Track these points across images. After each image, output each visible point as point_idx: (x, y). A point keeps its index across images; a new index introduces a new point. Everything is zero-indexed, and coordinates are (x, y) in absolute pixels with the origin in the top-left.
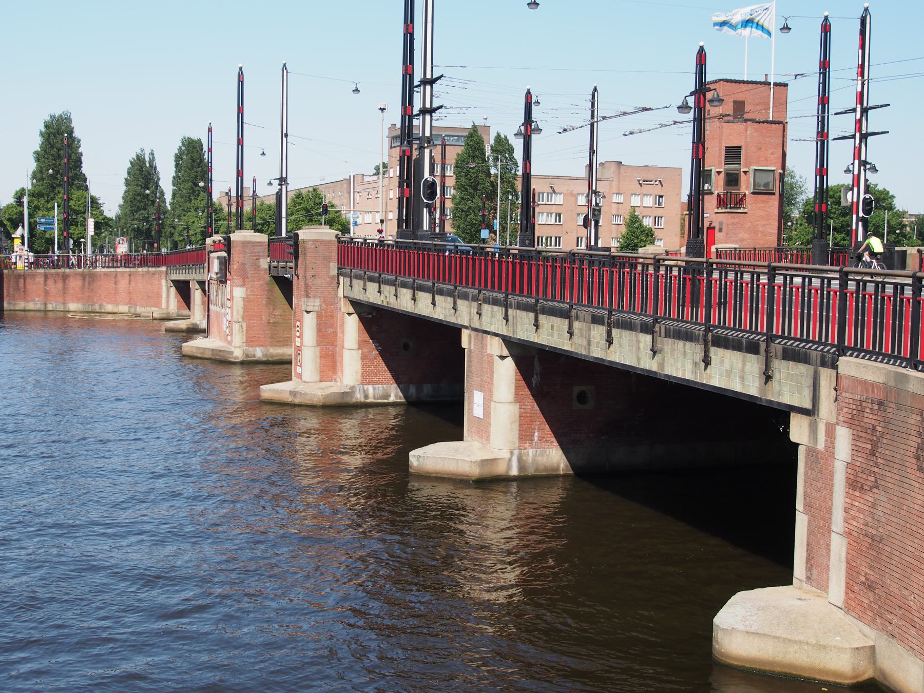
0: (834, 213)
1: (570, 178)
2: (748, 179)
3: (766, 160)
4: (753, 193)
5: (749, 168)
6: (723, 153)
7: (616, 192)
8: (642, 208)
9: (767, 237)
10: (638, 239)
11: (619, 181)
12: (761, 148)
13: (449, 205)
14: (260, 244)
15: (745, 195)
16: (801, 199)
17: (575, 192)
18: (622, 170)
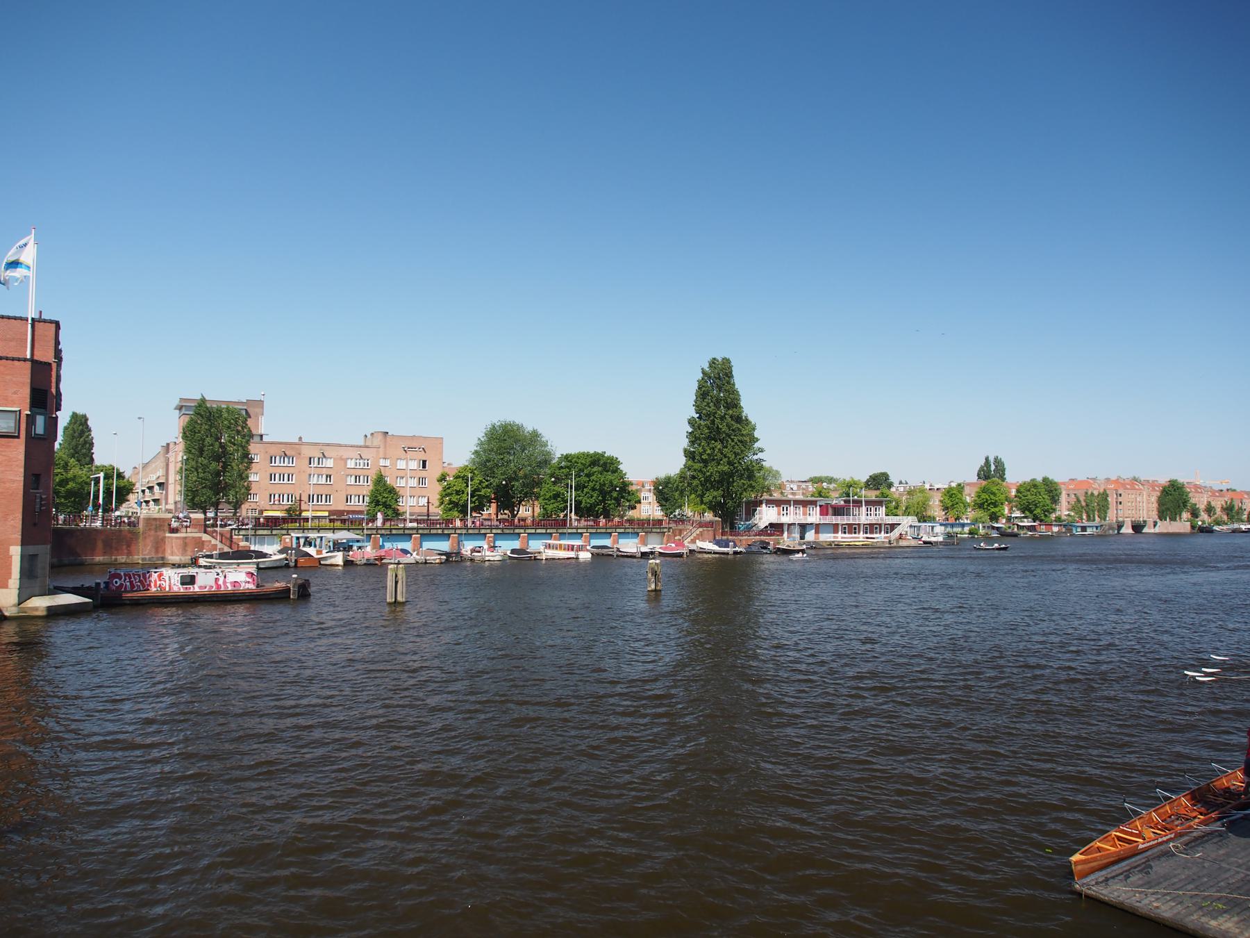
1: (340, 446)
9: (7, 485)
11: (385, 447)
17: (344, 457)
18: (388, 439)
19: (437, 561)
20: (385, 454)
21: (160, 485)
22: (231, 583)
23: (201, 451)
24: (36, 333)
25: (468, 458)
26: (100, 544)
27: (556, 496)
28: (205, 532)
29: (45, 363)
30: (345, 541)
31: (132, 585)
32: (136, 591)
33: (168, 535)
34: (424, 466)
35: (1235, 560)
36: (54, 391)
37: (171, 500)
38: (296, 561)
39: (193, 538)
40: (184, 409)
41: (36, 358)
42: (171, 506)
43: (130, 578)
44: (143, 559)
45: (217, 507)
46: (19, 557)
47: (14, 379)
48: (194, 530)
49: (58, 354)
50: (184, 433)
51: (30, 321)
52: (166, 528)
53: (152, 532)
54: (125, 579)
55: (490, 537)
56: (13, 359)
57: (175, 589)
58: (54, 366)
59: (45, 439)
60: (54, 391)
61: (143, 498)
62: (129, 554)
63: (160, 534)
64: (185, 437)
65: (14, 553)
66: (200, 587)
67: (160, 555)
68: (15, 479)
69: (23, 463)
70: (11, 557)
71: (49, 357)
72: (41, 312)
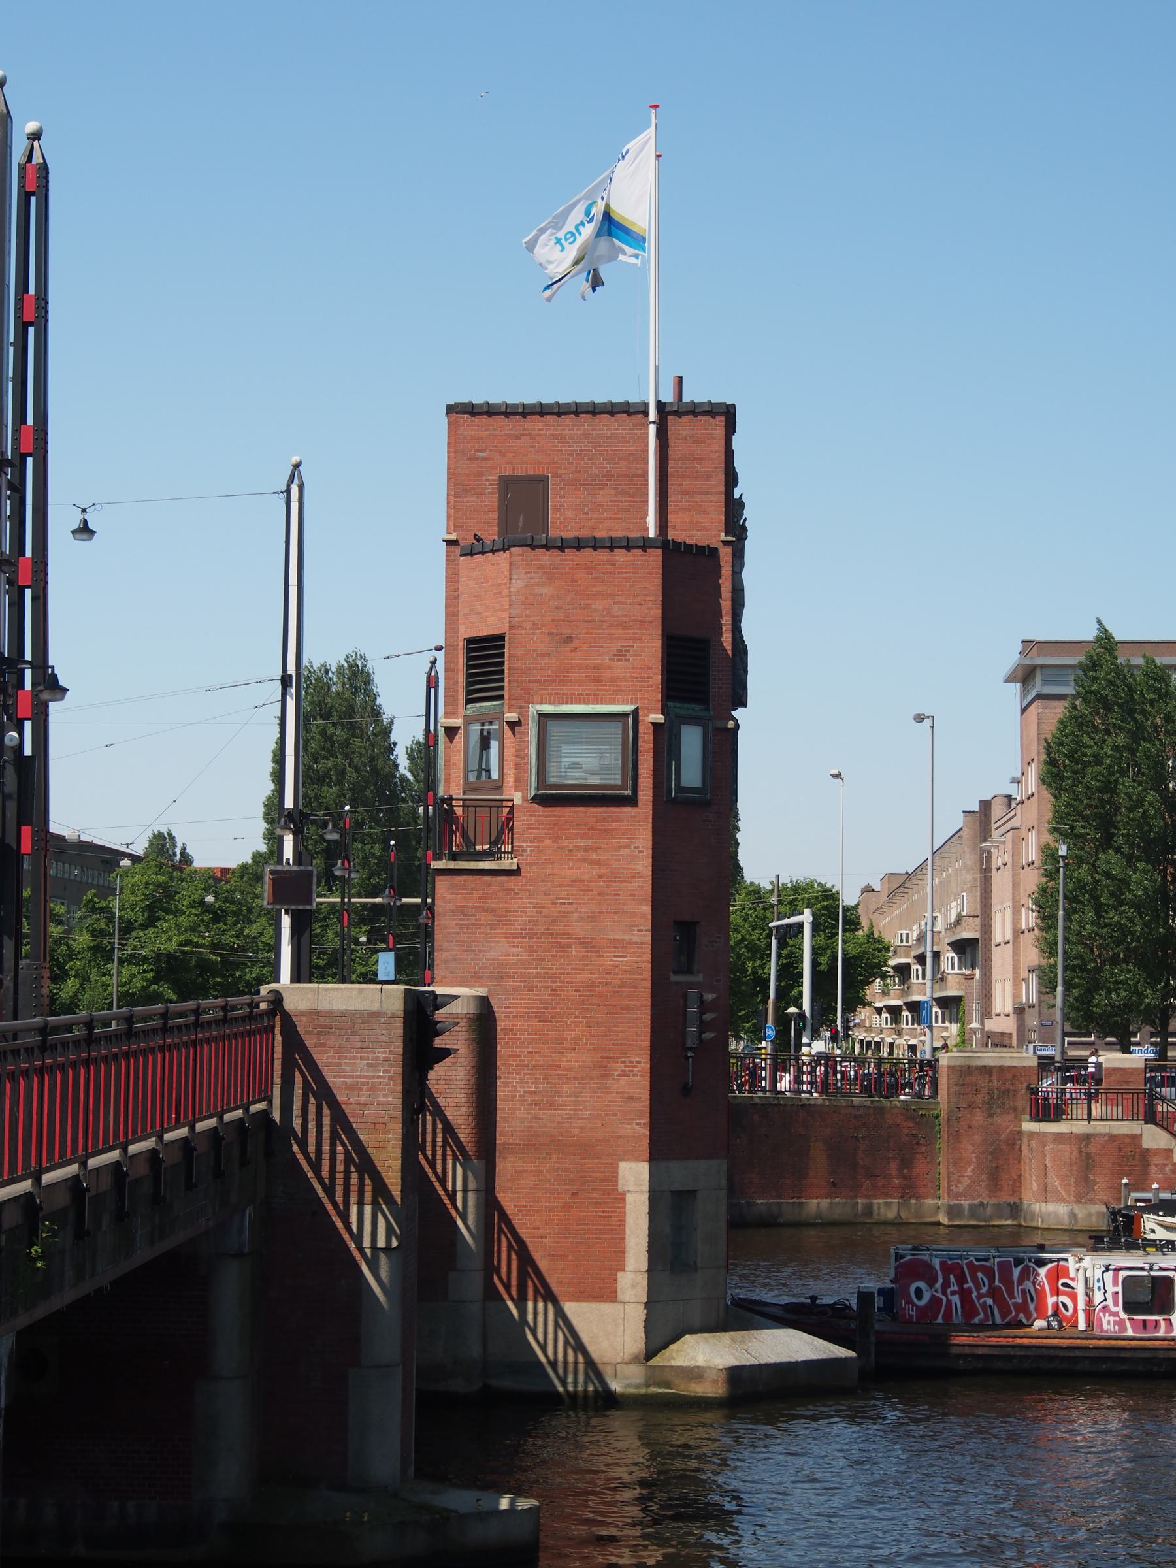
2: (521, 753)
3: (596, 679)
5: (523, 709)
9: (607, 960)
14: (647, 530)
21: (963, 947)
23: (1106, 825)
24: (671, 452)
26: (819, 1157)
28: (1151, 1117)
29: (701, 549)
31: (969, 1308)
32: (982, 1327)
33: (1028, 1126)
35: (1175, 1061)
36: (727, 640)
37: (1003, 1000)
39: (1113, 1138)
40: (1038, 679)
41: (672, 535)
42: (1004, 1024)
43: (961, 1280)
44: (953, 1211)
45: (1165, 1024)
46: (644, 1198)
47: (616, 610)
48: (1114, 1111)
49: (734, 510)
50: (1052, 762)
51: (652, 416)
52: (1023, 1102)
53: (979, 1118)
54: (946, 1284)
56: (612, 545)
57: (1108, 1324)
58: (725, 555)
59: (706, 804)
60: (727, 640)
61: (904, 993)
62: (909, 1190)
63: (1003, 1121)
64: (1053, 776)
65: (631, 1186)
67: (1006, 1198)
68: (627, 938)
69: (646, 886)
70: (622, 1198)
71: (713, 534)
72: (680, 381)
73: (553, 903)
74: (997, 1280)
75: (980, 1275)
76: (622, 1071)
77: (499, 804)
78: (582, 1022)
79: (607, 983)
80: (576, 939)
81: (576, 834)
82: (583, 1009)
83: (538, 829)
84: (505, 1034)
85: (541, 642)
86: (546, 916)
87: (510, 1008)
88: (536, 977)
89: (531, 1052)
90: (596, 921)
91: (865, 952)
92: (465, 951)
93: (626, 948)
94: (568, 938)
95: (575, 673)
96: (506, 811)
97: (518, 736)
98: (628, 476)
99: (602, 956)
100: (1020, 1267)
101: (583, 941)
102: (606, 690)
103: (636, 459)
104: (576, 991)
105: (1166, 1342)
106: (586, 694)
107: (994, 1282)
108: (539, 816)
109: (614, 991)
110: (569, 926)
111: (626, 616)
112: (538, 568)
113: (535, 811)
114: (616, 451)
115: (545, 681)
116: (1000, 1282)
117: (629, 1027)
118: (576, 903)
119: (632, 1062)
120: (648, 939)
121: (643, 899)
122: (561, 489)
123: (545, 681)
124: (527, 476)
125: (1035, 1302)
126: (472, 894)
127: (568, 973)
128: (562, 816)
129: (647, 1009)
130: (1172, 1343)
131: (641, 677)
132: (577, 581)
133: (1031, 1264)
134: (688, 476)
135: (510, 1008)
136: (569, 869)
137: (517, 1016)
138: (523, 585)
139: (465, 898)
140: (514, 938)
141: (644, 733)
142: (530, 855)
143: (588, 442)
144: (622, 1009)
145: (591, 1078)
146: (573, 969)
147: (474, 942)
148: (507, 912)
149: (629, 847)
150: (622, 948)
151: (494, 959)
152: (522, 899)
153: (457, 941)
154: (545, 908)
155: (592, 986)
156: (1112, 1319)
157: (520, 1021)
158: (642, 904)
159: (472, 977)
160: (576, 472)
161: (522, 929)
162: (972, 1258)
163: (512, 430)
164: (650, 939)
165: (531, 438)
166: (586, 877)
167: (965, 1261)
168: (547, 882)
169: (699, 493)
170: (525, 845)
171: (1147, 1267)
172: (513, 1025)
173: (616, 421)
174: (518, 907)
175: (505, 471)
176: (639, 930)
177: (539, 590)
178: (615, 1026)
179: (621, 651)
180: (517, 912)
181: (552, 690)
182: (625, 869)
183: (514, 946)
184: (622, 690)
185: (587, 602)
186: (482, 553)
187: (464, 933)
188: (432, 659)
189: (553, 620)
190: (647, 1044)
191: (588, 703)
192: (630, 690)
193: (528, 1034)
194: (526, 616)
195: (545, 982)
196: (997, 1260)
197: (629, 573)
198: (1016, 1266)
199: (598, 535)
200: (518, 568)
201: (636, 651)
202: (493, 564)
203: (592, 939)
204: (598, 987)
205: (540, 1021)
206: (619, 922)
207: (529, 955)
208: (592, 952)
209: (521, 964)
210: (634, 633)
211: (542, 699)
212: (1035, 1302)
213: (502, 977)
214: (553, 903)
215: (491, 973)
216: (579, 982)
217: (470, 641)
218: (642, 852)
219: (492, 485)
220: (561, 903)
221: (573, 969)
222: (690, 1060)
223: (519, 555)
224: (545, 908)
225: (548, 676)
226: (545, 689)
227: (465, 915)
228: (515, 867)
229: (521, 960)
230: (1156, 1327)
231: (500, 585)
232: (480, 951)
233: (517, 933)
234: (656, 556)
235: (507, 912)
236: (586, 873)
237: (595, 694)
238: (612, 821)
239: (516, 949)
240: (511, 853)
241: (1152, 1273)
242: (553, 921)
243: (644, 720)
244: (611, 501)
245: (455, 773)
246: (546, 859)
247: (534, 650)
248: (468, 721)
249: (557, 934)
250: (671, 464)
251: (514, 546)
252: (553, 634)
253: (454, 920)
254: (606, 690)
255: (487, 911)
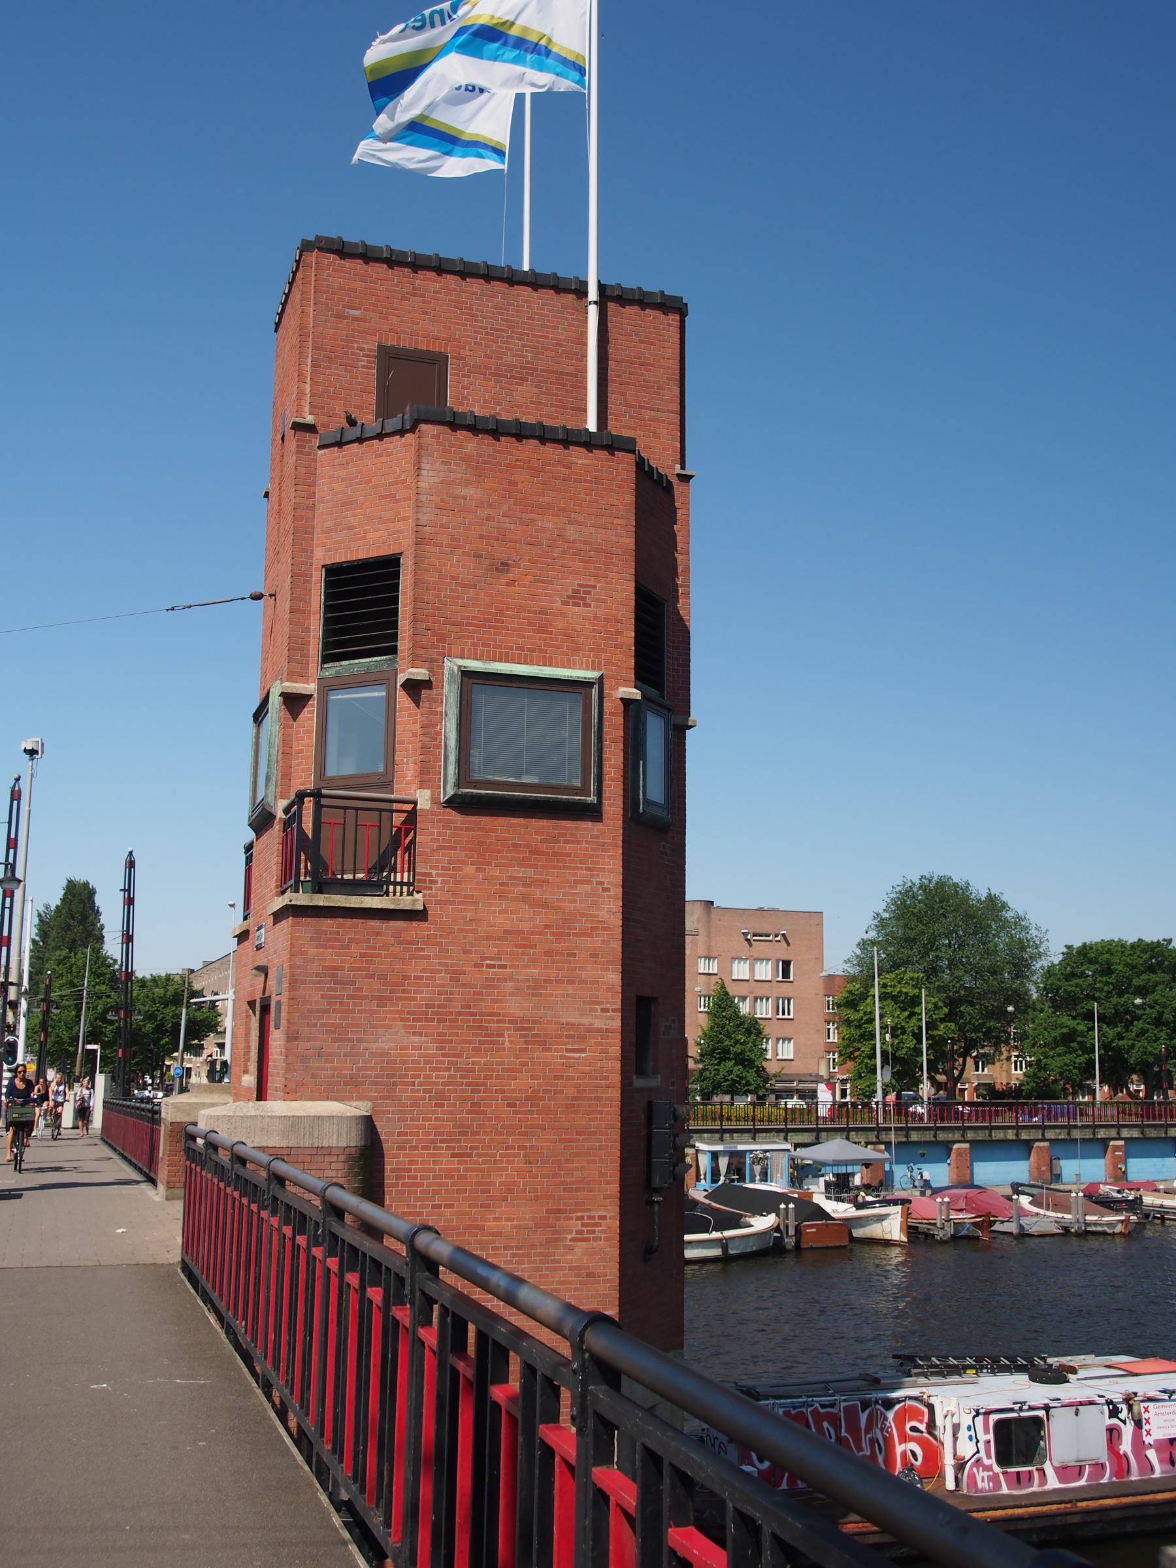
0: (1101, 990)
2: (430, 729)
3: (543, 629)
4: (459, 804)
5: (435, 664)
6: (317, 598)
7: (704, 954)
8: (752, 983)
9: (556, 1057)
10: (729, 1037)
11: (709, 934)
12: (504, 567)
13: (27, 945)
15: (412, 817)
16: (1040, 964)
18: (714, 915)
19: (1119, 1228)
20: (709, 948)
22: (1160, 1446)
25: (849, 955)
27: (1068, 1038)
30: (810, 1162)
34: (786, 974)
38: (798, 1229)
47: (572, 532)
55: (1117, 1148)
57: (983, 1481)
66: (1063, 1472)
68: (586, 1021)
73: (476, 965)
74: (843, 1430)
75: (825, 1424)
76: (578, 1232)
77: (385, 808)
78: (518, 1155)
79: (556, 1092)
80: (510, 1022)
81: (513, 858)
82: (521, 1134)
83: (454, 848)
84: (397, 1178)
85: (463, 566)
86: (464, 986)
87: (406, 1134)
88: (449, 1084)
89: (439, 1206)
90: (540, 995)
91: (207, 1017)
92: (335, 1040)
93: (584, 1037)
94: (498, 1022)
95: (512, 616)
96: (398, 819)
97: (424, 704)
98: (555, 372)
99: (549, 1050)
100: (867, 1412)
101: (521, 1026)
102: (557, 647)
103: (565, 352)
104: (509, 1105)
105: (1063, 1506)
106: (529, 650)
107: (841, 1432)
108: (456, 828)
109: (567, 1106)
110: (500, 1001)
111: (585, 542)
112: (461, 459)
113: (450, 821)
114: (541, 337)
115: (468, 625)
116: (846, 1432)
117: (589, 1162)
118: (511, 967)
119: (593, 1218)
120: (617, 1023)
121: (609, 963)
122: (464, 376)
123: (468, 625)
124: (417, 351)
125: (883, 1453)
126: (349, 947)
127: (498, 1077)
128: (491, 830)
129: (616, 1133)
130: (1069, 1505)
131: (607, 632)
132: (516, 484)
133: (878, 1407)
134: (634, 385)
135: (406, 1134)
136: (501, 912)
137: (416, 1148)
138: (437, 480)
139: (338, 954)
140: (415, 1020)
141: (611, 714)
142: (442, 889)
143: (503, 320)
144: (578, 1133)
145: (532, 1247)
146: (507, 1070)
147: (352, 1026)
148: (405, 978)
149: (589, 882)
150: (579, 1037)
151: (382, 1055)
152: (427, 957)
153: (323, 1025)
154: (463, 972)
155: (533, 1098)
156: (986, 1474)
157: (422, 1155)
158: (607, 970)
159: (346, 1084)
160: (486, 356)
161: (427, 1006)
162: (817, 1405)
163: (397, 286)
164: (620, 1023)
165: (424, 302)
166: (526, 926)
167: (810, 1409)
168: (466, 931)
169: (647, 408)
170: (434, 872)
171: (1017, 1407)
172: (410, 1162)
173: (541, 298)
174: (423, 971)
175: (387, 340)
176: (603, 1010)
177: (462, 491)
178: (567, 1161)
179: (578, 592)
180: (421, 978)
181: (479, 639)
182: (582, 915)
183: (415, 1034)
184: (579, 649)
185: (531, 516)
186: (360, 440)
187: (335, 1011)
188: (16, 776)
189: (481, 537)
190: (614, 1188)
191: (532, 664)
192: (591, 650)
193: (434, 1177)
194: (442, 526)
195: (462, 1091)
196: (843, 1404)
197: (591, 482)
198: (863, 1411)
199: (548, 422)
200: (431, 455)
201: (599, 594)
202: (380, 455)
203: (534, 1022)
204: (543, 1099)
205: (453, 1156)
206: (574, 996)
207: (438, 1049)
208: (533, 1043)
209: (426, 1062)
210: (597, 568)
211: (463, 650)
212: (883, 1453)
213: (395, 1084)
214: (476, 965)
215: (377, 1076)
216: (514, 1091)
217: (333, 571)
218: (608, 890)
219: (368, 356)
220: (489, 966)
221: (507, 1070)
222: (656, 1207)
223: (433, 436)
224: (463, 972)
225: (474, 618)
226: (469, 637)
227: (336, 983)
228: (421, 908)
229: (426, 1055)
230: (1029, 1480)
231: (391, 484)
232: (360, 1040)
233: (421, 1013)
234: (628, 463)
235: (405, 978)
236: (526, 919)
237: (540, 651)
238: (566, 842)
239: (417, 1038)
240: (409, 884)
241: (1022, 1414)
242: (475, 993)
243: (610, 695)
244: (532, 402)
245: (300, 764)
246: (466, 896)
247: (453, 578)
248: (327, 687)
249: (482, 1014)
250: (611, 365)
251: (427, 422)
252: (480, 556)
253: (321, 989)
254: (557, 647)
255: (372, 976)
